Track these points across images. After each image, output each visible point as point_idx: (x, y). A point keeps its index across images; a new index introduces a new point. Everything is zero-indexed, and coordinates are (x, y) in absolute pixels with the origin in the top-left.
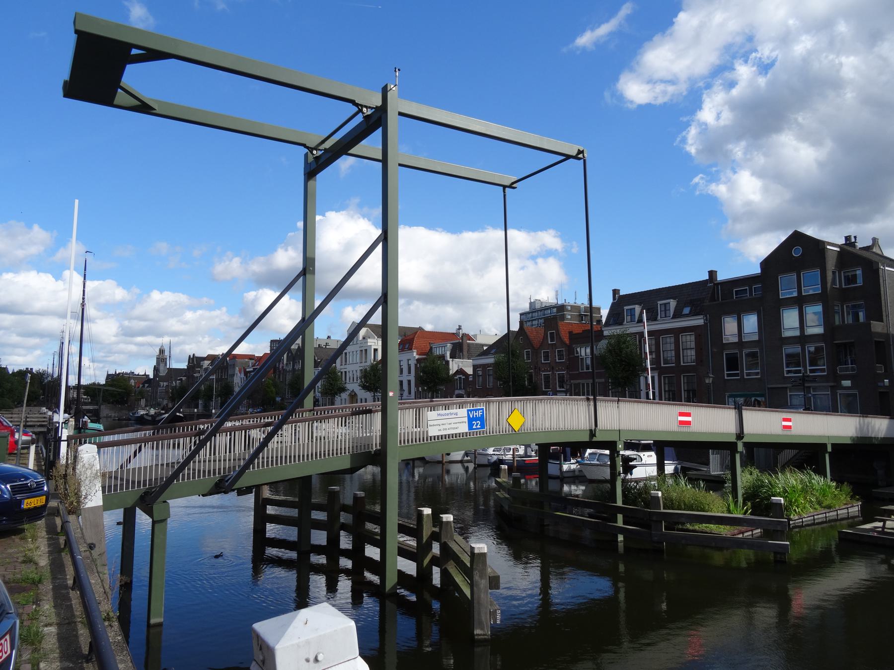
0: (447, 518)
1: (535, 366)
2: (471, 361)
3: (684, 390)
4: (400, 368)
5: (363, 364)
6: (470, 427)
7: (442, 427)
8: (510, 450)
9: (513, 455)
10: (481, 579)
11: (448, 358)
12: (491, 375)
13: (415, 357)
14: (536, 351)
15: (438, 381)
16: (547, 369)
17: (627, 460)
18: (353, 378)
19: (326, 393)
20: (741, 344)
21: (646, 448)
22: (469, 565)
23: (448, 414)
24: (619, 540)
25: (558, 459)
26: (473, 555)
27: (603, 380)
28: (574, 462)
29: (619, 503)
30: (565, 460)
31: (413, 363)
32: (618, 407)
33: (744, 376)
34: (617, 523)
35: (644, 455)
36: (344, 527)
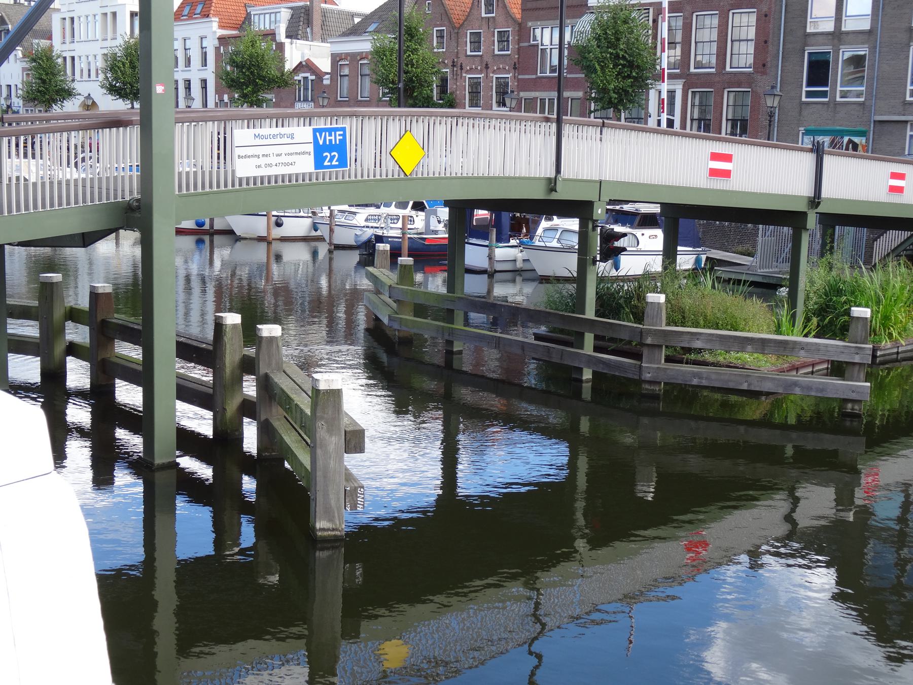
0: (270, 331)
1: (453, 62)
2: (329, 45)
3: (727, 120)
4: (186, 54)
5: (109, 43)
6: (319, 163)
7: (263, 161)
8: (398, 219)
9: (403, 229)
10: (331, 435)
11: (282, 36)
12: (366, 75)
13: (215, 32)
14: (456, 31)
15: (260, 82)
16: (476, 68)
17: (609, 238)
18: (89, 71)
19: (35, 99)
20: (838, 36)
21: (648, 221)
22: (308, 411)
23: (274, 136)
24: (584, 378)
25: (485, 237)
26: (316, 393)
27: (580, 94)
28: (516, 244)
29: (590, 313)
30: (499, 240)
31: (211, 45)
32: (601, 140)
33: (835, 97)
34: (584, 314)
35: (643, 234)
36: (73, 350)
